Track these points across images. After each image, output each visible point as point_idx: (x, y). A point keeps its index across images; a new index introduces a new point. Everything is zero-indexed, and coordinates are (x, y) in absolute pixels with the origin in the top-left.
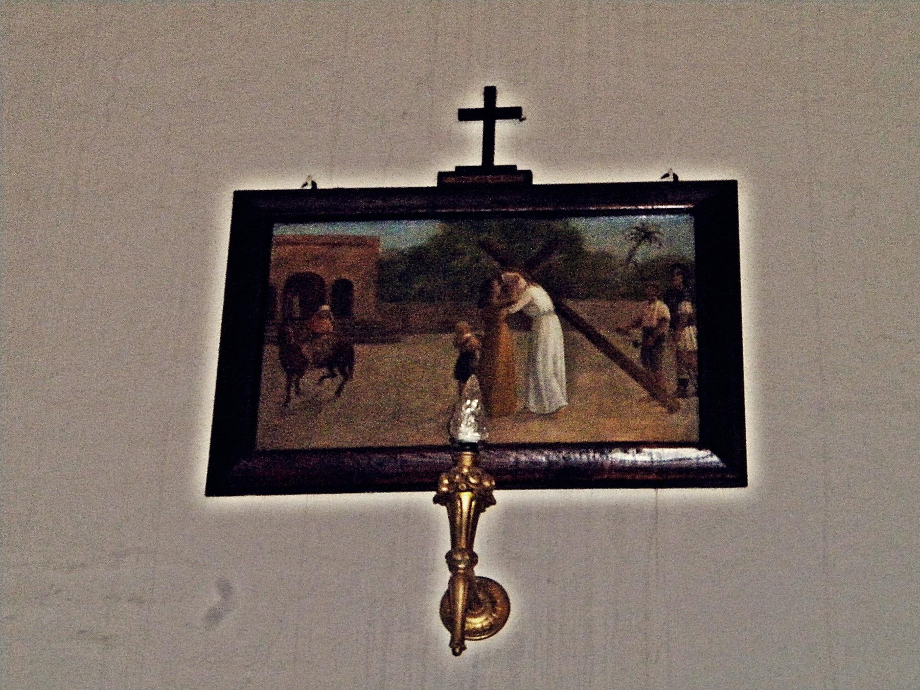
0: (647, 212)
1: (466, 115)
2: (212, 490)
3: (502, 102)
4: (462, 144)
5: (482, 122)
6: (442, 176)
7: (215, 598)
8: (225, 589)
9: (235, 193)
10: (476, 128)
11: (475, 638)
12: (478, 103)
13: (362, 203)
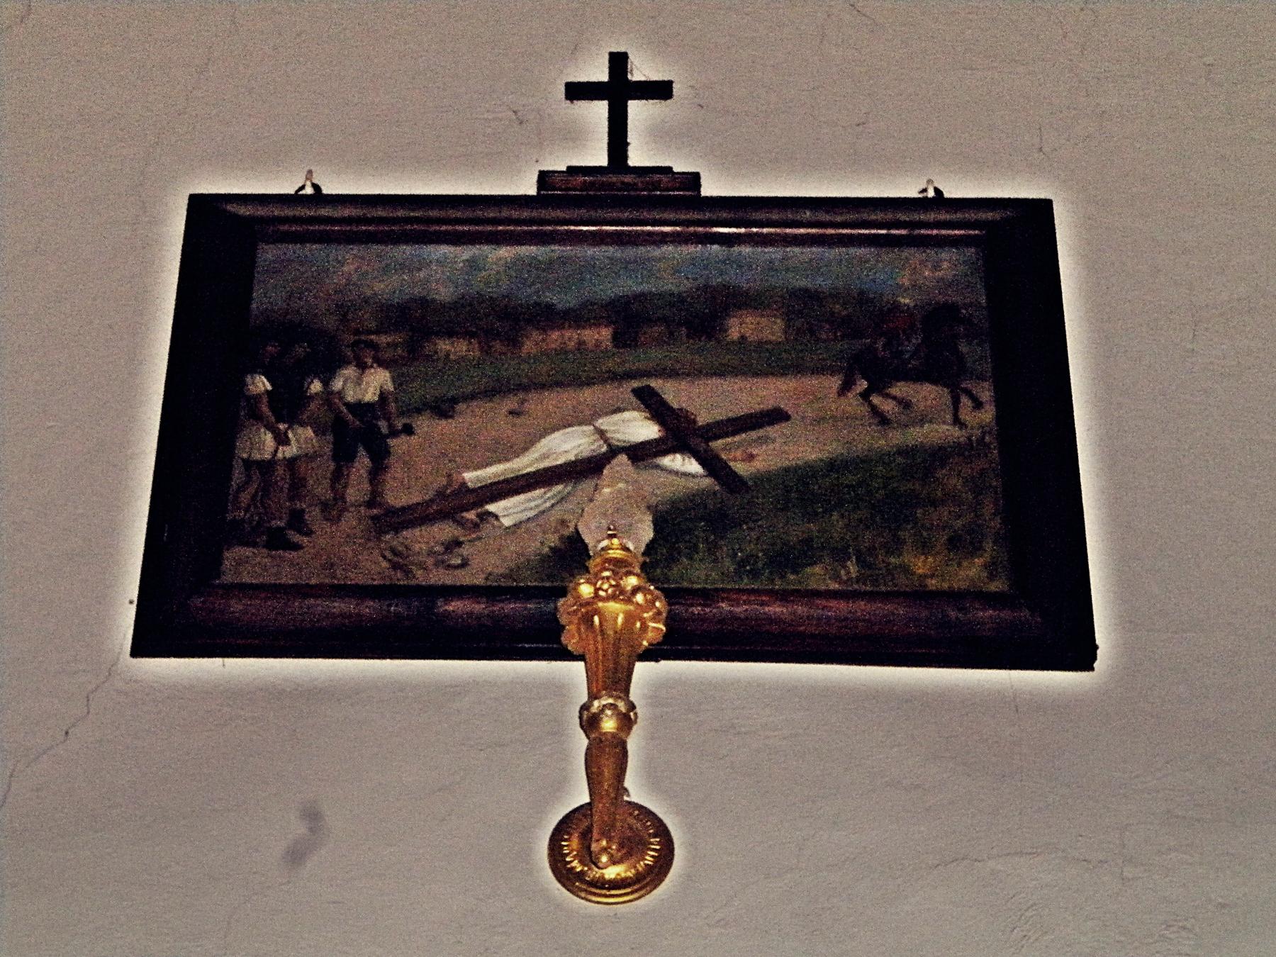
0: (618, 239)
1: (577, 91)
2: (137, 651)
3: (640, 71)
4: (574, 136)
5: (630, 103)
6: (545, 178)
7: (299, 829)
8: (312, 816)
12: (601, 74)
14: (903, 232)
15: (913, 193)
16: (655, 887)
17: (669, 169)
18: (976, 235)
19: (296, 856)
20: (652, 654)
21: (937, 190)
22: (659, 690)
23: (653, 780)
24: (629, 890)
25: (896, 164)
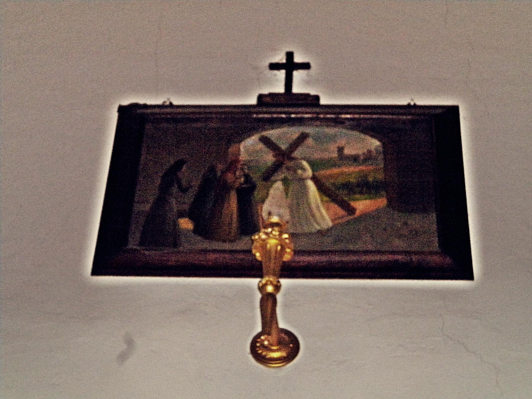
1: (274, 67)
2: (95, 272)
3: (297, 59)
4: (270, 82)
10: (282, 74)
11: (390, 257)
14: (333, 116)
19: (123, 357)
23: (286, 319)
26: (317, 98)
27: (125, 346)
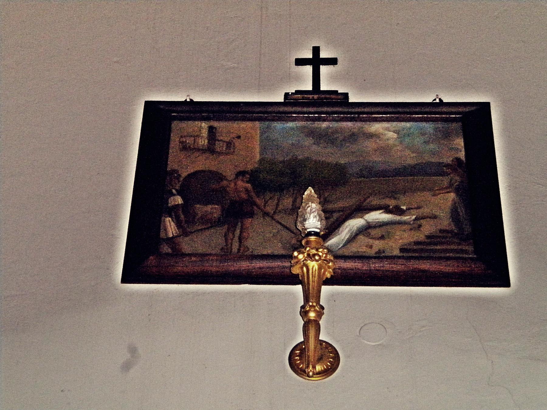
1: (300, 62)
2: (507, 284)
3: (323, 55)
4: (298, 78)
8: (133, 350)
9: (145, 101)
10: (308, 69)
12: (309, 55)
13: (225, 108)
15: (430, 100)
16: (331, 375)
17: (335, 92)
18: (451, 115)
19: (127, 367)
20: (328, 282)
21: (440, 99)
22: (332, 297)
24: (318, 376)
25: (424, 88)
26: (346, 95)
27: (129, 356)
